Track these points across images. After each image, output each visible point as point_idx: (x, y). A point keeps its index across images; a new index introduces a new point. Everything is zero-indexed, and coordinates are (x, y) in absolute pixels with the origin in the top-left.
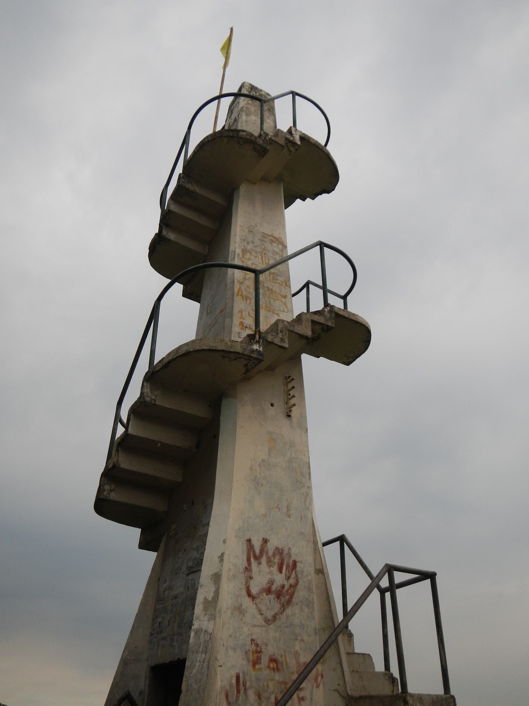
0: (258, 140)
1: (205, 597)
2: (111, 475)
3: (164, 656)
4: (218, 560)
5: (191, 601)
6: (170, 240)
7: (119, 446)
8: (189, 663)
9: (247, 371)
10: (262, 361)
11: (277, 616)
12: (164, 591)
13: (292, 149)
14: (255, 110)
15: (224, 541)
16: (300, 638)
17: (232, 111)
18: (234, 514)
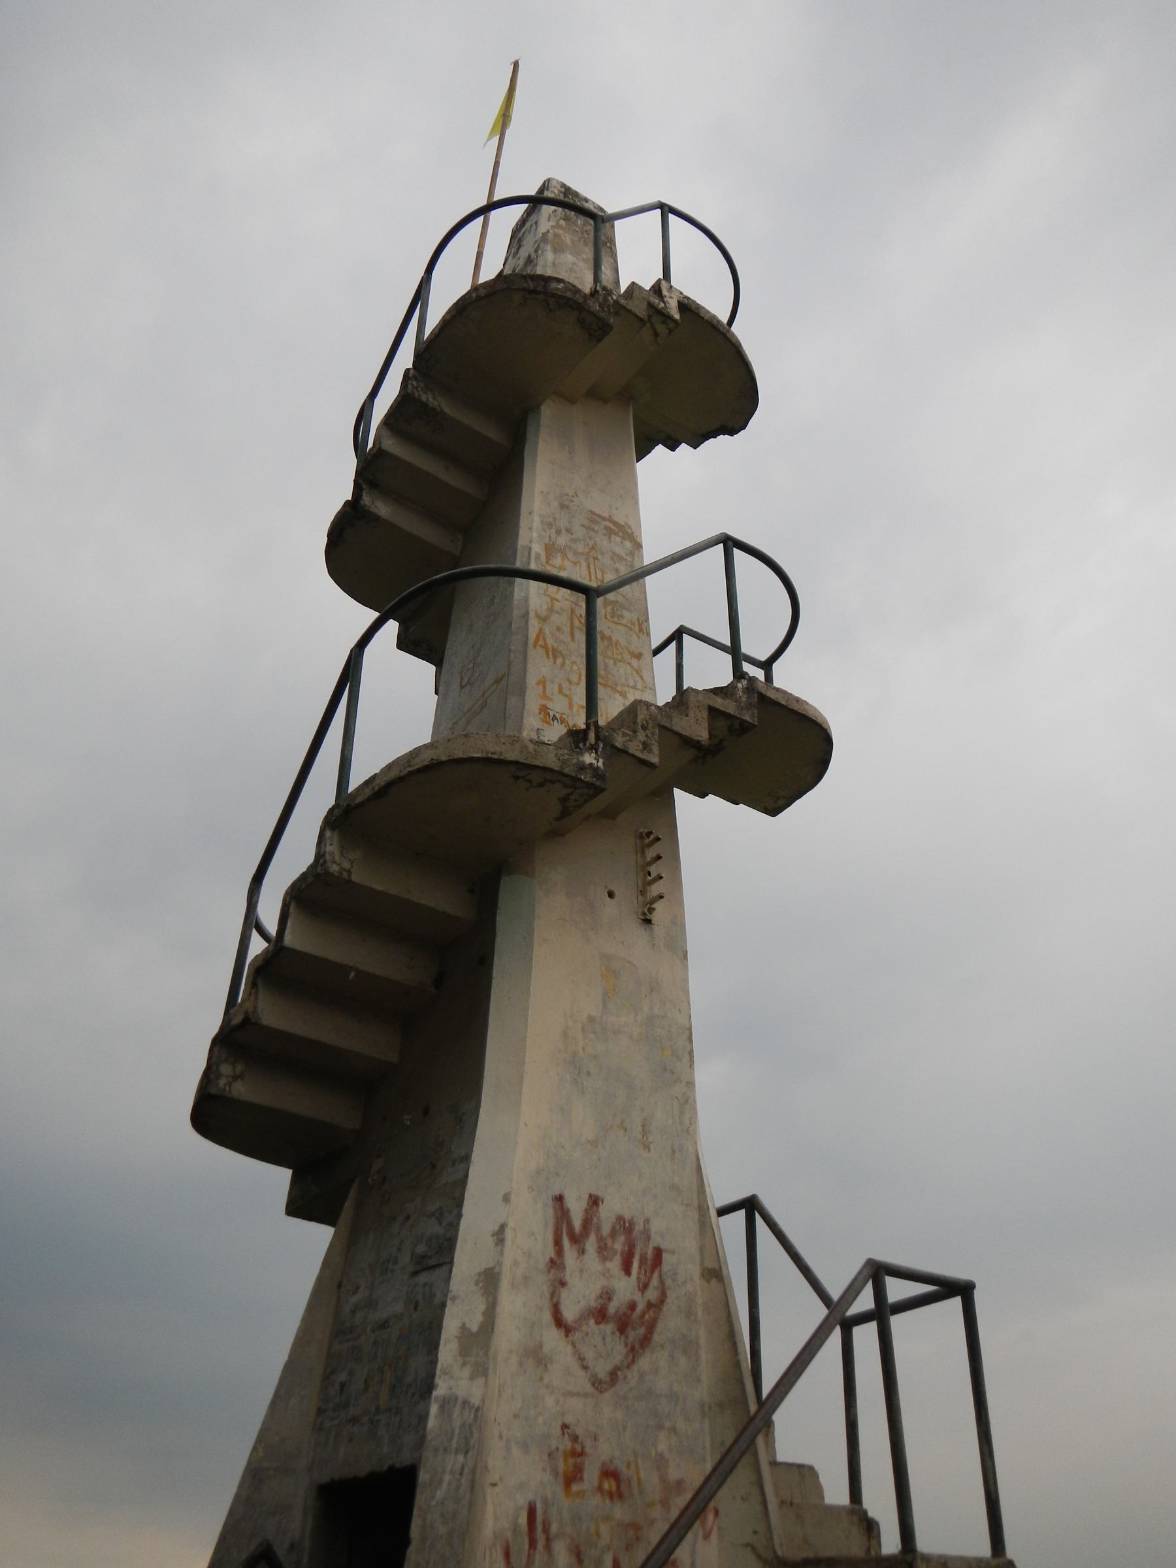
0: (590, 302)
1: (464, 1324)
2: (236, 1041)
3: (357, 1458)
4: (490, 1241)
5: (429, 1334)
6: (378, 518)
7: (272, 972)
8: (427, 1476)
9: (565, 813)
10: (604, 790)
11: (619, 1373)
12: (353, 1312)
13: (661, 328)
14: (572, 241)
15: (506, 1198)
16: (668, 1424)
17: (520, 240)
18: (525, 1141)
